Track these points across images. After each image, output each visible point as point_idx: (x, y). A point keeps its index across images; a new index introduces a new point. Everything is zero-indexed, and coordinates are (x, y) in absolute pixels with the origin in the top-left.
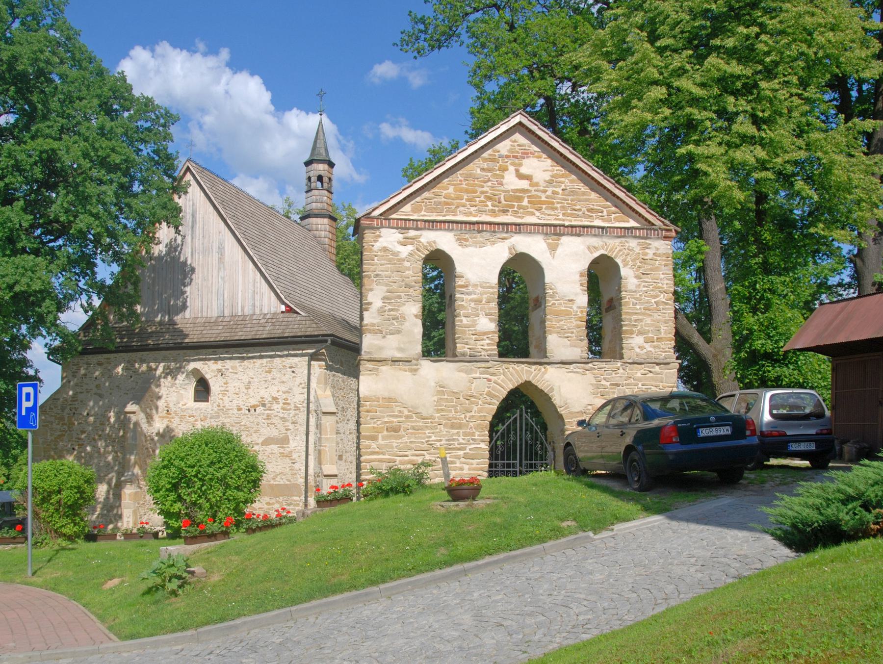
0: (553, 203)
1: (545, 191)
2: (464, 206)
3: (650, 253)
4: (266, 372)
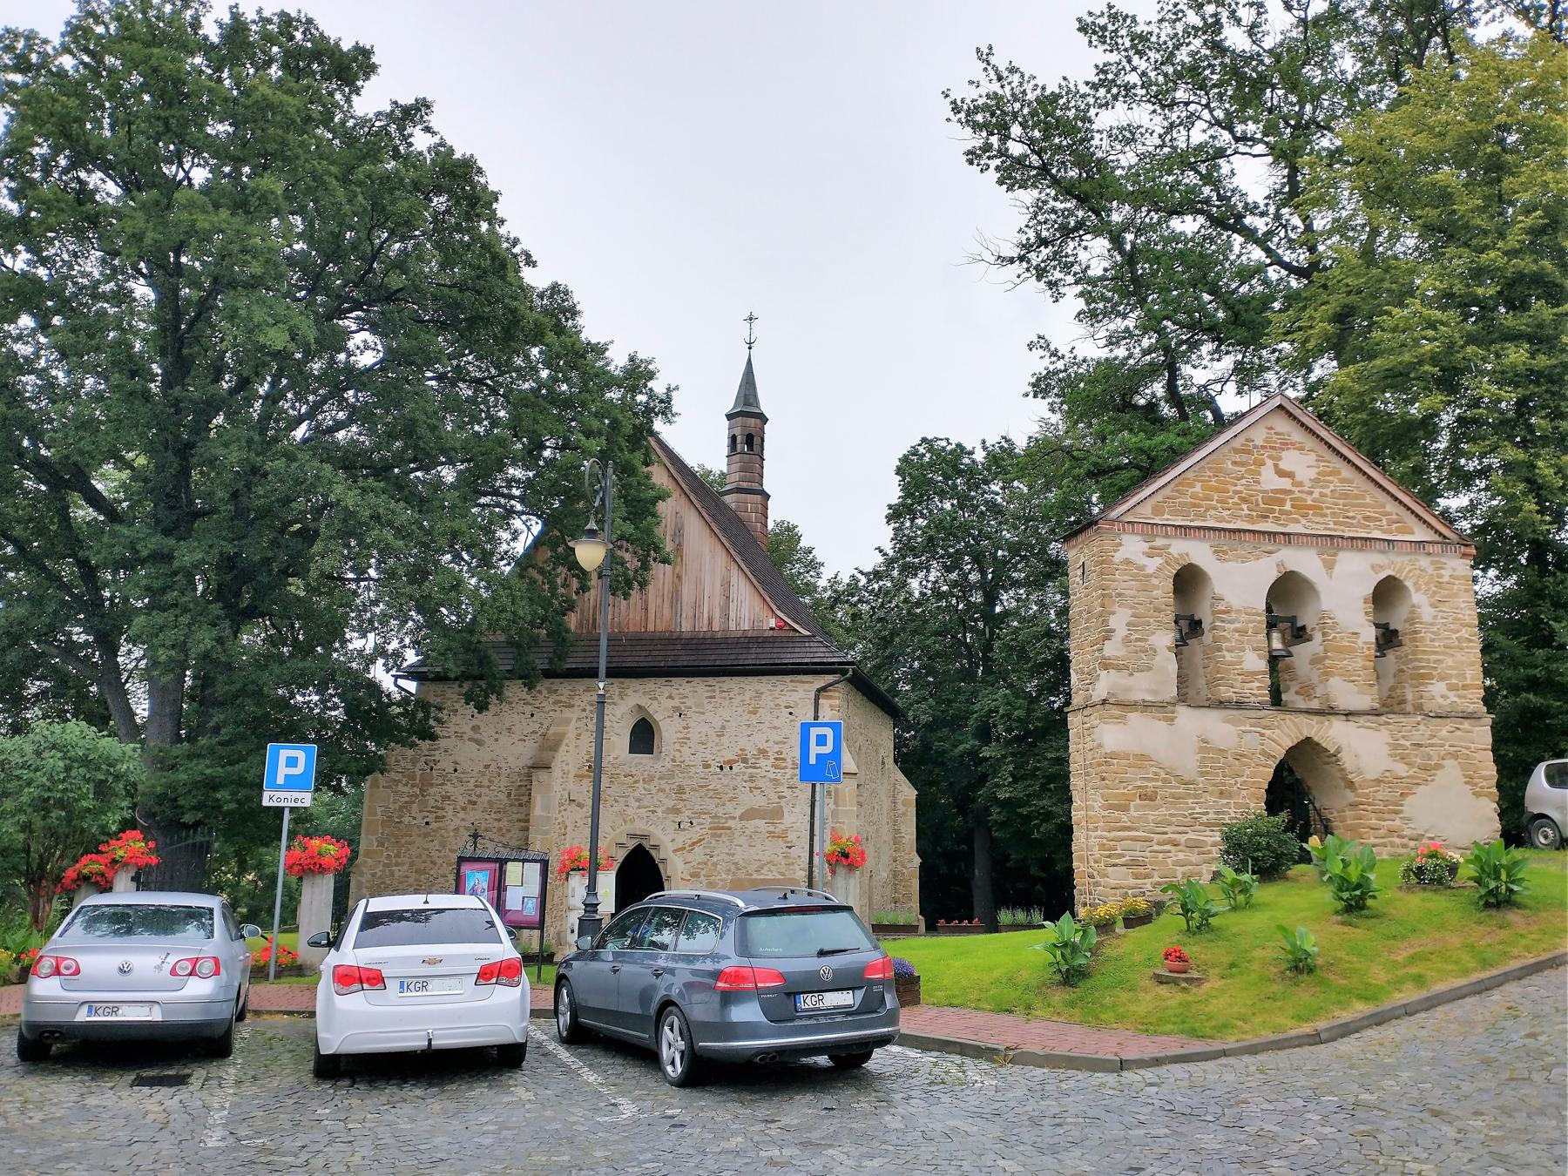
0: (1321, 508)
1: (1311, 493)
2: (1215, 509)
3: (1446, 574)
4: (750, 712)
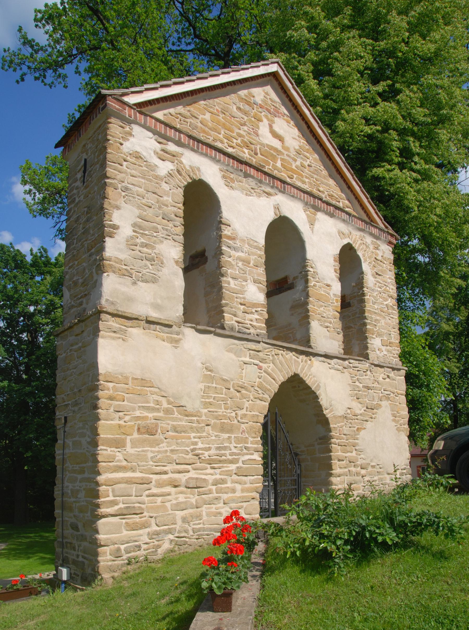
0: (302, 176)
